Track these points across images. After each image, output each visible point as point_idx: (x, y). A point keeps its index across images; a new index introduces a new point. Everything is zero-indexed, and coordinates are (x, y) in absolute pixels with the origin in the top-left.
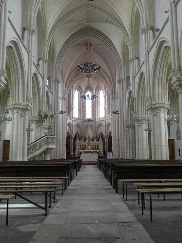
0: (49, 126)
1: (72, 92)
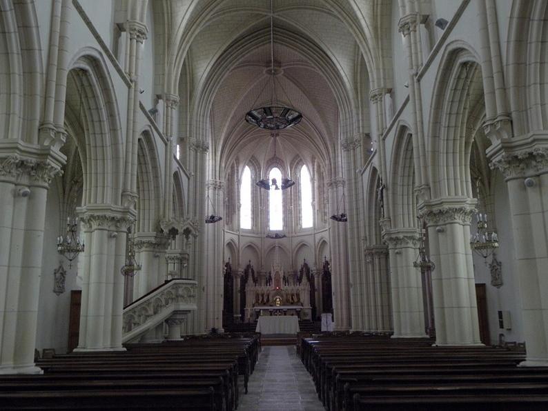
0: (180, 254)
1: (238, 170)
